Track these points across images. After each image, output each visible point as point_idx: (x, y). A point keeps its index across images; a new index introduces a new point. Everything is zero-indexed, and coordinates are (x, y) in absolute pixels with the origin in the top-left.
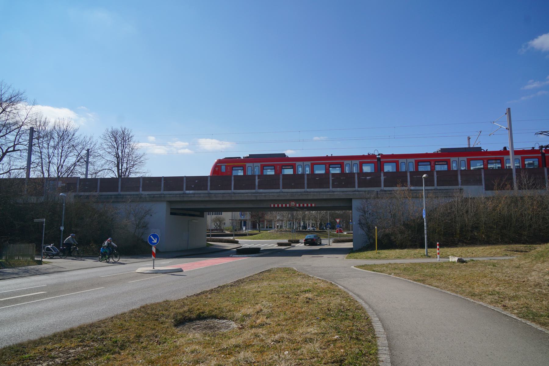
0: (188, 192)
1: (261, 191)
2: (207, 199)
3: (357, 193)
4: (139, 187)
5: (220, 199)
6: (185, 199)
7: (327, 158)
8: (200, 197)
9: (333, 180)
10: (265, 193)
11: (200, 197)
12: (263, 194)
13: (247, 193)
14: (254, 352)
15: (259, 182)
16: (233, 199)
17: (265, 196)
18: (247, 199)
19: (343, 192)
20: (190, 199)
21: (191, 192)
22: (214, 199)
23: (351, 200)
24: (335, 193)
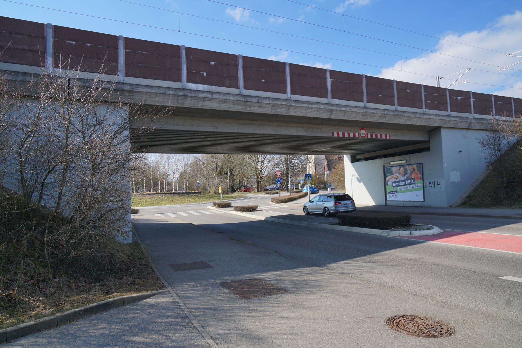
0: (192, 86)
1: (337, 101)
2: (239, 108)
3: (453, 119)
4: (44, 52)
5: (266, 110)
6: (188, 104)
7: (154, 58)
8: (225, 101)
9: (425, 95)
10: (346, 106)
11: (225, 101)
12: (343, 109)
13: (317, 103)
14: (38, 307)
15: (332, 84)
16: (292, 113)
17: (345, 112)
18: (314, 115)
19: (439, 116)
20: (200, 105)
21: (201, 87)
22: (255, 109)
23: (437, 129)
24: (432, 117)
